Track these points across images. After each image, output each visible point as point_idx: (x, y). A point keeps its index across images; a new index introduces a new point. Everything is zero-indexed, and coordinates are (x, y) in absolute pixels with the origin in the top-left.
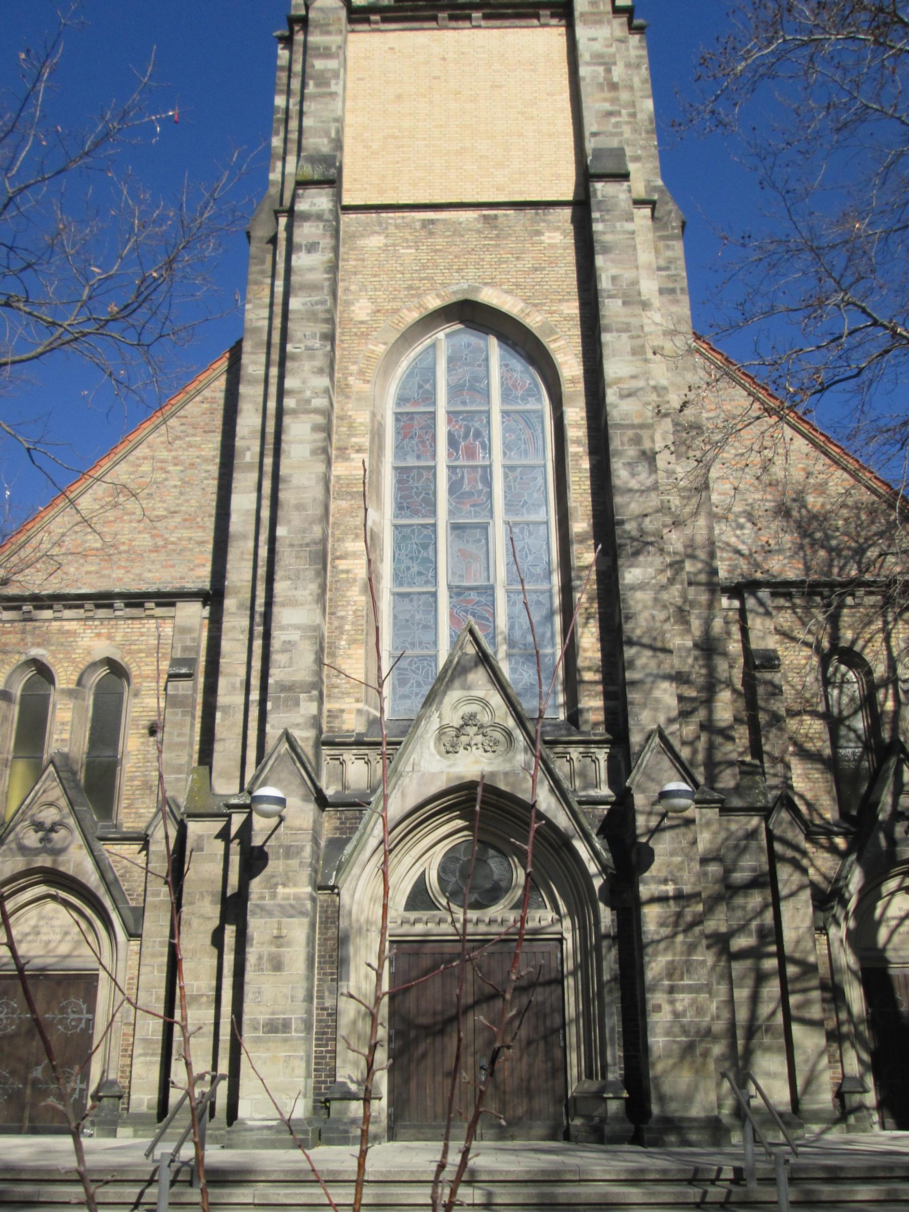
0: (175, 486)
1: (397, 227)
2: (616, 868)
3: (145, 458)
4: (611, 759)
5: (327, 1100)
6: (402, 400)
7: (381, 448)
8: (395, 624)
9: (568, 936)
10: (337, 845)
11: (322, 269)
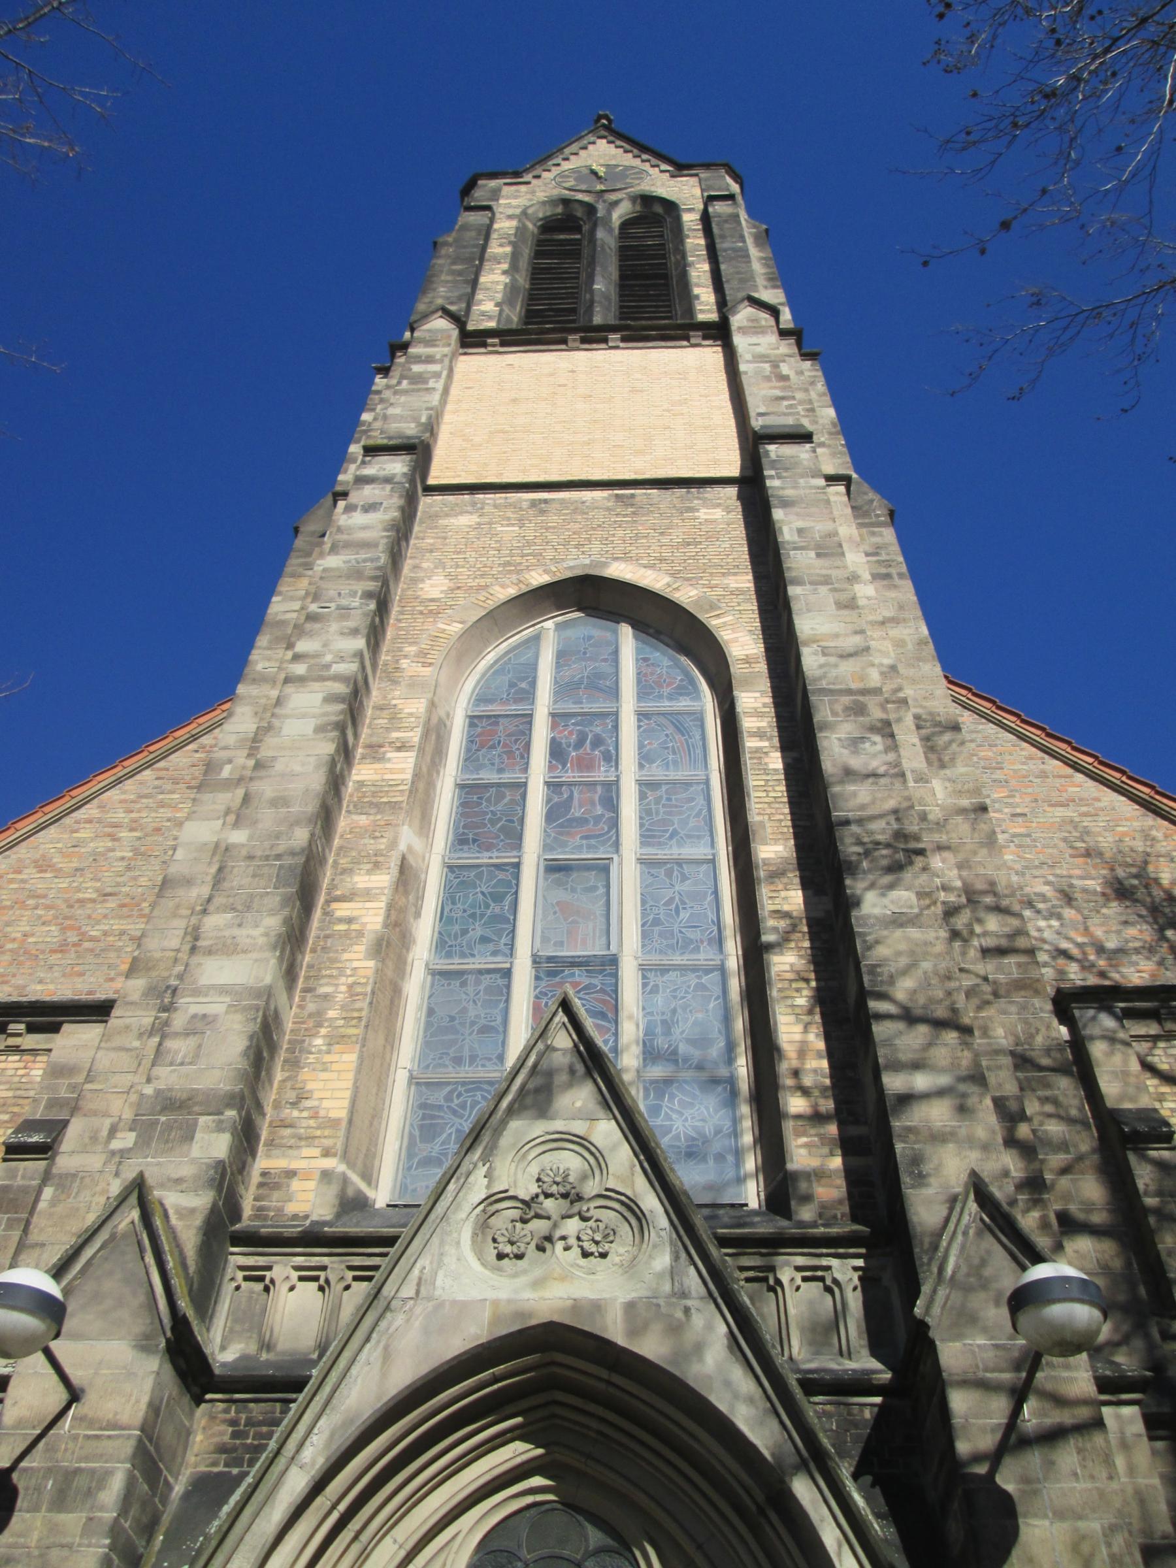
0: (123, 858)
1: (495, 506)
3: (90, 821)
4: (868, 1280)
6: (481, 698)
7: (439, 753)
8: (428, 1025)
10: (210, 1490)
11: (380, 527)
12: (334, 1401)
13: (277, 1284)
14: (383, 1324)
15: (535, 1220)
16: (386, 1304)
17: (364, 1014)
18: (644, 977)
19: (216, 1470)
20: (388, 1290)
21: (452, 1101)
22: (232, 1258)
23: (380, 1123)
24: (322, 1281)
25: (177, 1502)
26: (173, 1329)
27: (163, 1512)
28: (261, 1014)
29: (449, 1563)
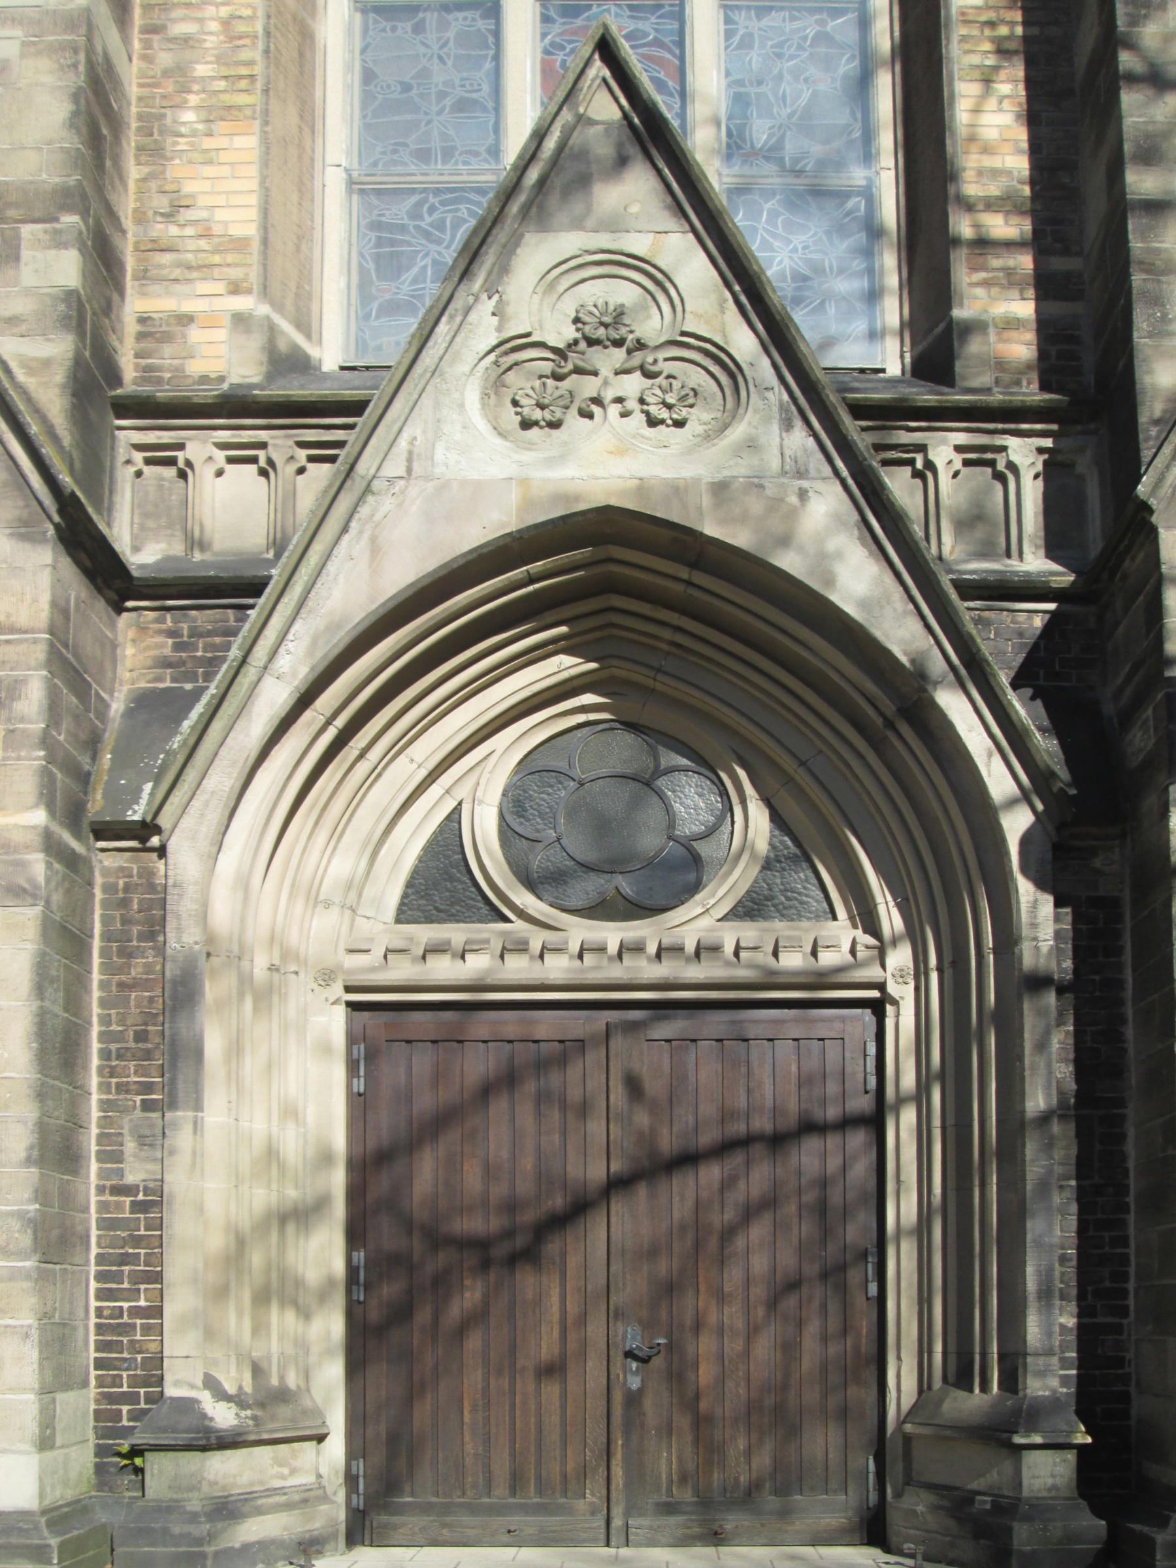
2: (1076, 780)
4: (1055, 470)
5: (136, 1451)
8: (367, 98)
9: (903, 992)
10: (158, 708)
12: (310, 603)
13: (197, 466)
14: (364, 511)
15: (574, 376)
16: (364, 484)
17: (258, 69)
18: (728, 20)
19: (162, 686)
20: (365, 467)
21: (421, 218)
22: (121, 435)
23: (311, 249)
24: (262, 462)
25: (118, 719)
26: (61, 512)
27: (105, 730)
28: (82, 57)
29: (483, 781)
